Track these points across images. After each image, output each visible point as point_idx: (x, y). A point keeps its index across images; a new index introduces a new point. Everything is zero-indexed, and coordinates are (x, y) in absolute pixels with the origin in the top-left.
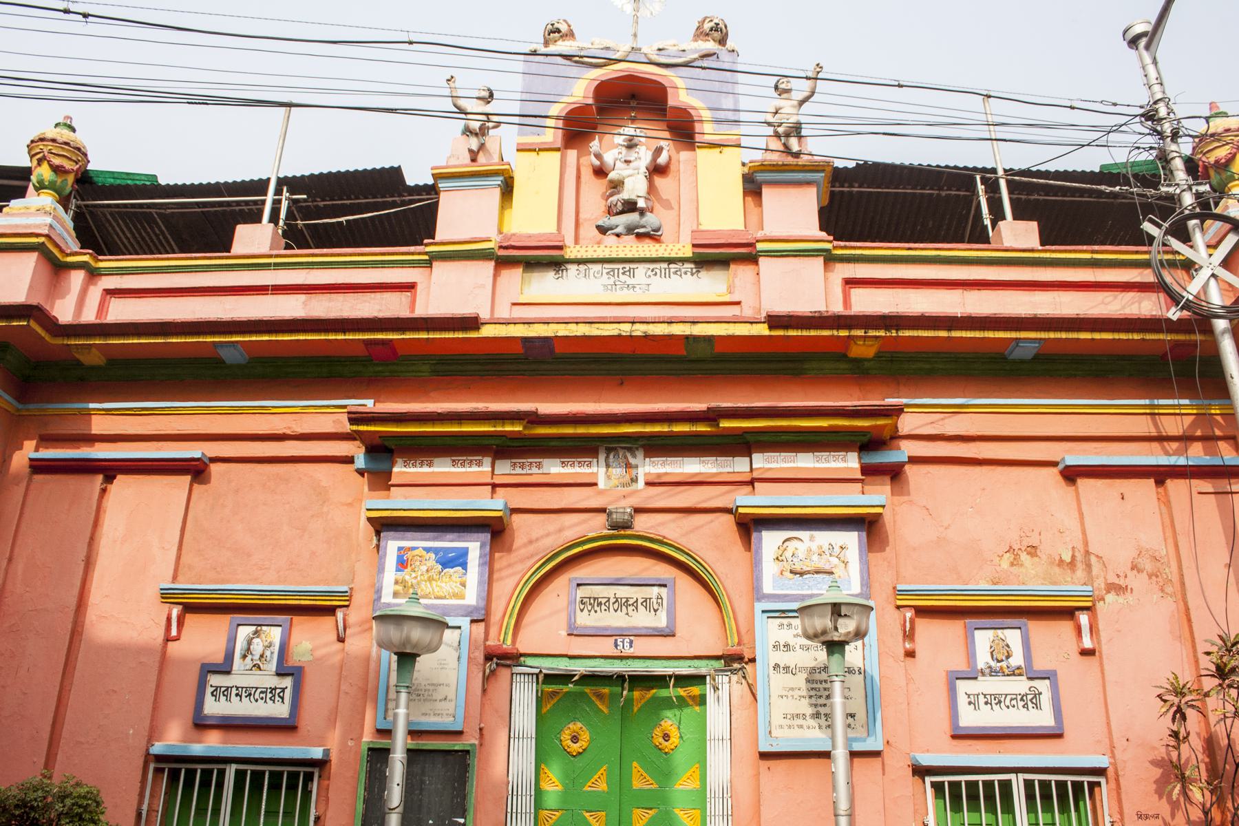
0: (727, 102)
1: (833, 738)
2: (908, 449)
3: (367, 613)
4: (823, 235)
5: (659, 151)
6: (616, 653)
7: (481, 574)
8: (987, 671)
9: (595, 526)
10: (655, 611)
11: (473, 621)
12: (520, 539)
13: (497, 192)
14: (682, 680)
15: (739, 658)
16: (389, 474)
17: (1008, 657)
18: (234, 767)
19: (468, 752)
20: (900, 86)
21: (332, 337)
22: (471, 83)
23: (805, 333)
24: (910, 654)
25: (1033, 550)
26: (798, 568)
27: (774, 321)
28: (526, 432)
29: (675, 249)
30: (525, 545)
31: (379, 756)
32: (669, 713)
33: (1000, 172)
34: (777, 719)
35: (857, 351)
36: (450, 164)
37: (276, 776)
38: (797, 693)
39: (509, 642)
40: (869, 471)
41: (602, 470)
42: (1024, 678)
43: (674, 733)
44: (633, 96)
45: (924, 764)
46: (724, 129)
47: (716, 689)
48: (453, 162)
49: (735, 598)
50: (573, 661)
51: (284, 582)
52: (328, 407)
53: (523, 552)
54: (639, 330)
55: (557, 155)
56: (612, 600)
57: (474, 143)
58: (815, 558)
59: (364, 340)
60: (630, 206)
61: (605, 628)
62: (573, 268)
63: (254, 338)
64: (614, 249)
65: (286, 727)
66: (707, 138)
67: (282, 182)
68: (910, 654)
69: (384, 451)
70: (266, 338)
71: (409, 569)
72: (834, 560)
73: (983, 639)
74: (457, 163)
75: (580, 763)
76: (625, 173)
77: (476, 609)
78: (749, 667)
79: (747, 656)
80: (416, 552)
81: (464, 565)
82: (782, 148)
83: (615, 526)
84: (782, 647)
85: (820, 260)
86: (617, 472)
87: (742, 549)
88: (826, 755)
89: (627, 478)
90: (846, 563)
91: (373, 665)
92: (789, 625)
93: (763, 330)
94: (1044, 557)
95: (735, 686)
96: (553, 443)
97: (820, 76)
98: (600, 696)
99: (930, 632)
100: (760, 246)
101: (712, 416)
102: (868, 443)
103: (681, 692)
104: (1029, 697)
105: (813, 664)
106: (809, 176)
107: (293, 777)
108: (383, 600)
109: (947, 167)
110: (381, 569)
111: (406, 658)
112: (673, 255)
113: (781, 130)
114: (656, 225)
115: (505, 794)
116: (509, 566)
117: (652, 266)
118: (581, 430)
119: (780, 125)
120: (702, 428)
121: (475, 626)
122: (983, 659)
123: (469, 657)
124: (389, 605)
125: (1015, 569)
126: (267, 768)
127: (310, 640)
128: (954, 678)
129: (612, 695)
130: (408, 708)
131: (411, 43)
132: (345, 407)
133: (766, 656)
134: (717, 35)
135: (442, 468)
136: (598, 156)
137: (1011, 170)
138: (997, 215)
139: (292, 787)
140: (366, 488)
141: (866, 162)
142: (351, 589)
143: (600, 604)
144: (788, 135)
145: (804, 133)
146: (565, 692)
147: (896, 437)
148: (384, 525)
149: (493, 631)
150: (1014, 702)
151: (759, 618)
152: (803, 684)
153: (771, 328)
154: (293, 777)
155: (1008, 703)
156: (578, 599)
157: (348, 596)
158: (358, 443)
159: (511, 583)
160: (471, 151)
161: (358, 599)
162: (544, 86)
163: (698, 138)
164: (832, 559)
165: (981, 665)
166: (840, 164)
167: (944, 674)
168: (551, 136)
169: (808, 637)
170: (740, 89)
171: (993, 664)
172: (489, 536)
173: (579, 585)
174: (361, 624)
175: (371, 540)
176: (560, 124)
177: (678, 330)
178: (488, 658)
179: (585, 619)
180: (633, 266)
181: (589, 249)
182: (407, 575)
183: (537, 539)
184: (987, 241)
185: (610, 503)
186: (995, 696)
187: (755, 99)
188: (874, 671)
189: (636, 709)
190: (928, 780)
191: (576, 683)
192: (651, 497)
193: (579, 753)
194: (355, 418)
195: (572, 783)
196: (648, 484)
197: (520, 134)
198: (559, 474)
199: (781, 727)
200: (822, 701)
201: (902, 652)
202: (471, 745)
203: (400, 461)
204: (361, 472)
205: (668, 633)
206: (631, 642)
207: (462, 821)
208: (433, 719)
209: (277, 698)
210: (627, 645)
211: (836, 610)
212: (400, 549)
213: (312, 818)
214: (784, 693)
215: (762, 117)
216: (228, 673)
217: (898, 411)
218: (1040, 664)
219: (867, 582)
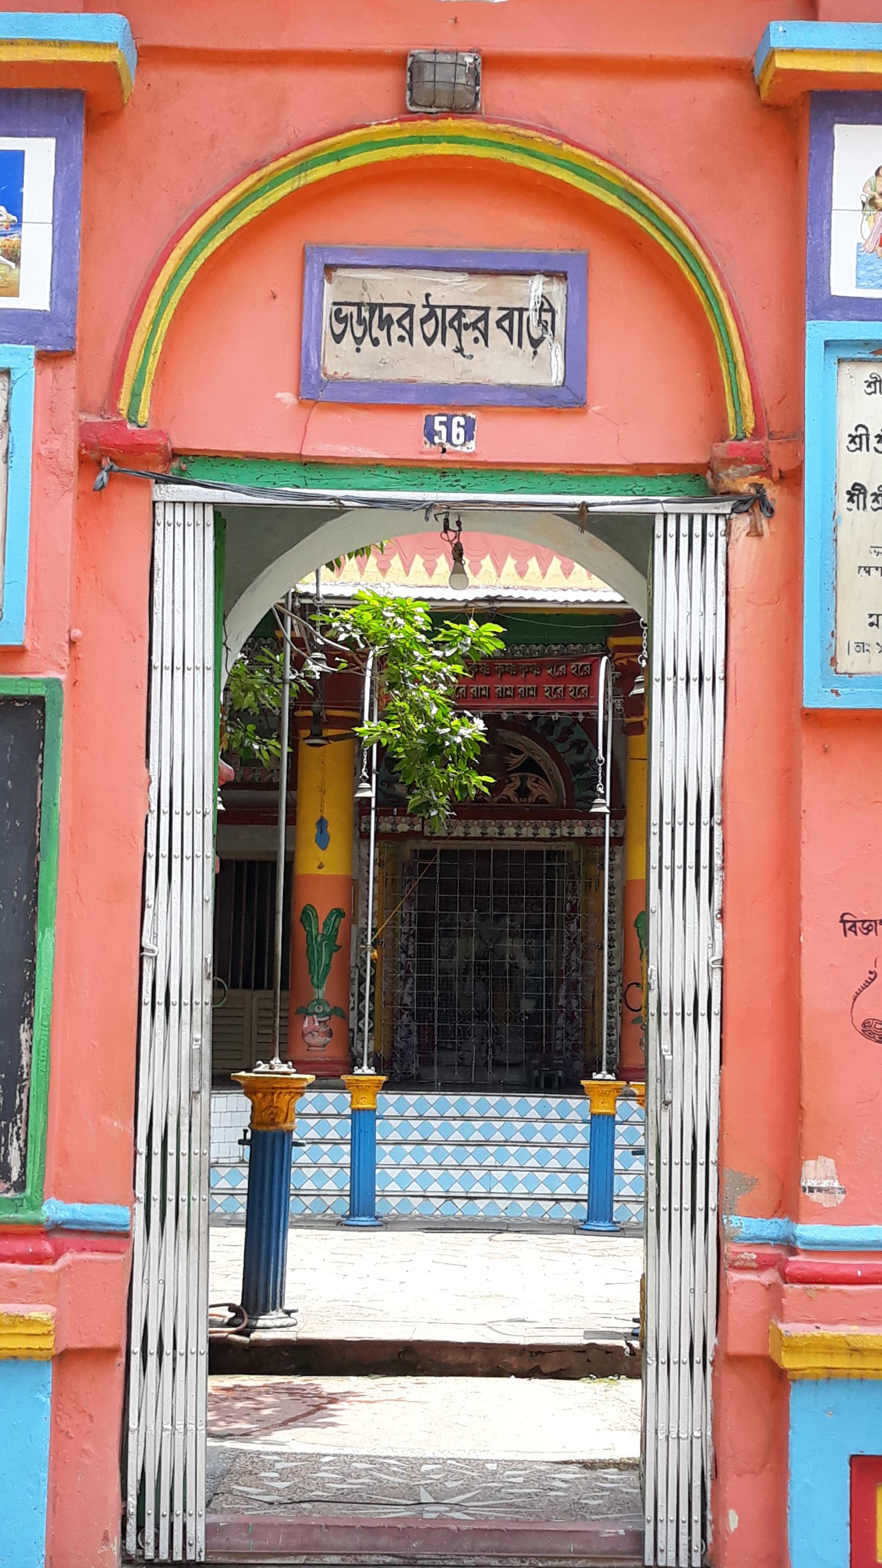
6: (429, 452)
10: (535, 343)
19: (39, 702)
34: (852, 626)
56: (420, 313)
123: (37, 455)
143: (386, 323)
156: (328, 308)
179: (342, 360)
199: (862, 647)
202: (48, 683)
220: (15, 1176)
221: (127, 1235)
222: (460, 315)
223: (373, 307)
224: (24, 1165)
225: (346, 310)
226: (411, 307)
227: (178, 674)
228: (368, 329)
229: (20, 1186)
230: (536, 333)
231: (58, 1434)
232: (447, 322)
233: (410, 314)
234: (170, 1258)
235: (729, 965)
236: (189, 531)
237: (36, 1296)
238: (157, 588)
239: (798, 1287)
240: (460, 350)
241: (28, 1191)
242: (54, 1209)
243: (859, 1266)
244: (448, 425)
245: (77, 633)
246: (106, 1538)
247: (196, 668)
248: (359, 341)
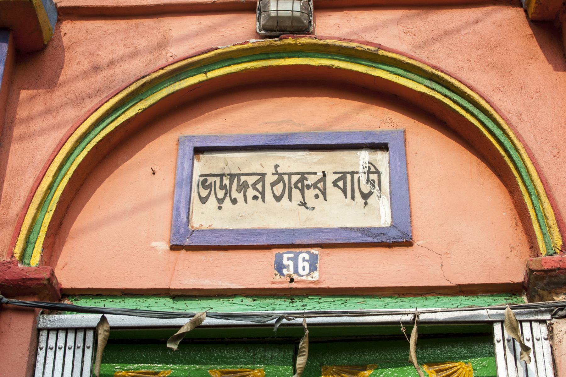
6: (281, 283)
10: (366, 196)
12: (74, 64)
30: (85, 74)
39: (35, 259)
53: (80, 86)
56: (270, 179)
116: (48, 111)
143: (243, 187)
156: (196, 178)
159: (49, 142)
173: (198, 151)
179: (208, 217)
183: (111, 64)
205: (397, 240)
223: (232, 177)
225: (210, 180)
226: (263, 175)
228: (228, 192)
230: (366, 189)
232: (298, 185)
236: (69, 353)
240: (303, 204)
244: (295, 260)
248: (220, 201)
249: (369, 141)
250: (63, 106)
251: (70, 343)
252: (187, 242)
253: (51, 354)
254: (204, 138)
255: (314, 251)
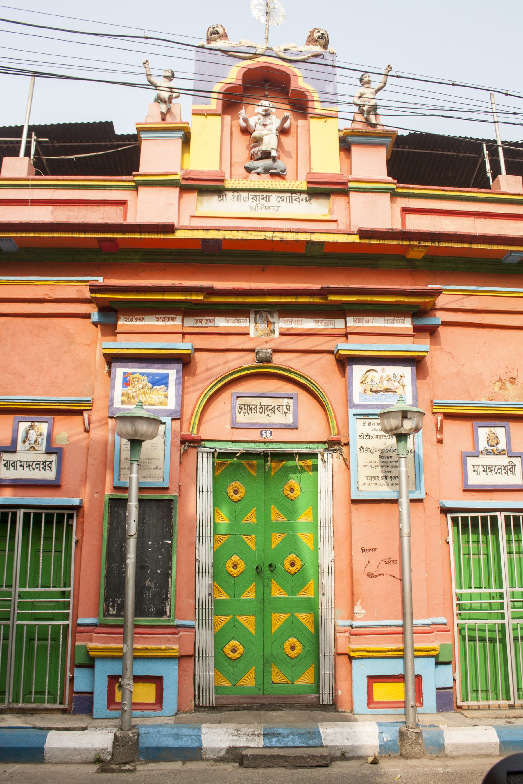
0: (329, 88)
1: (399, 492)
2: (441, 316)
3: (104, 413)
4: (390, 179)
5: (285, 119)
6: (262, 439)
7: (177, 390)
8: (485, 452)
9: (248, 361)
10: (286, 413)
11: (173, 419)
12: (200, 368)
13: (180, 142)
14: (304, 456)
15: (338, 443)
16: (115, 326)
17: (497, 444)
18: (22, 511)
19: (172, 500)
20: (453, 85)
21: (76, 235)
22: (159, 66)
23: (382, 242)
24: (440, 441)
25: (513, 381)
26: (374, 388)
27: (363, 234)
28: (205, 300)
29: (296, 185)
30: (204, 372)
31: (118, 504)
32: (294, 476)
33: (499, 143)
34: (362, 480)
35: (412, 255)
36: (148, 121)
37: (49, 517)
38: (374, 464)
39: (195, 432)
40: (418, 330)
41: (252, 325)
42: (506, 456)
43: (297, 488)
44: (266, 81)
45: (448, 507)
46: (328, 106)
47: (324, 461)
48: (149, 120)
49: (335, 406)
50: (234, 444)
51: (48, 394)
52: (73, 281)
53: (203, 376)
54: (278, 236)
55: (219, 118)
56: (259, 407)
57: (164, 108)
58: (385, 382)
59: (98, 238)
60: (266, 155)
61: (255, 424)
62: (230, 194)
63: (24, 235)
64: (257, 183)
65: (53, 486)
66: (317, 111)
67: (32, 128)
68: (440, 441)
69: (111, 312)
70: (32, 235)
71: (131, 386)
72: (397, 384)
73: (483, 433)
74: (152, 121)
75: (239, 506)
76: (264, 132)
77: (175, 412)
78: (344, 449)
79: (343, 441)
80: (135, 376)
81: (166, 384)
82: (364, 121)
83: (261, 361)
84: (367, 437)
85: (388, 196)
86: (262, 326)
87: (339, 376)
88: (395, 501)
89: (268, 331)
90: (403, 386)
91: (109, 447)
92: (369, 423)
93: (355, 239)
94: (519, 385)
95: (336, 460)
96: (221, 308)
97: (390, 74)
98: (251, 466)
99: (452, 428)
100: (351, 185)
101: (323, 293)
102: (418, 312)
103: (301, 463)
104: (509, 467)
105: (383, 447)
106: (382, 140)
107: (60, 517)
108: (115, 406)
109: (466, 138)
110: (113, 387)
111: (136, 443)
112: (295, 188)
113: (365, 108)
114: (283, 169)
115: (194, 526)
116: (194, 385)
117: (281, 195)
118: (240, 300)
119: (364, 105)
120: (316, 300)
121: (174, 422)
122: (483, 445)
123: (171, 442)
124: (118, 409)
125: (502, 392)
126: (44, 511)
127: (67, 431)
128: (465, 456)
129: (258, 465)
130: (138, 473)
131: (146, 38)
132: (87, 281)
133: (356, 442)
134: (322, 42)
135: (150, 322)
136: (245, 120)
137: (506, 142)
138: (496, 172)
139: (60, 523)
140: (99, 335)
141: (421, 133)
142: (93, 399)
143: (251, 409)
144: (368, 113)
145: (378, 111)
146: (231, 463)
147: (434, 309)
148: (112, 359)
149: (185, 425)
150: (500, 471)
151: (351, 418)
152: (377, 459)
153: (361, 238)
154: (60, 517)
155: (496, 471)
156: (237, 406)
157: (90, 403)
158: (94, 305)
159: (195, 395)
160: (162, 113)
161: (97, 405)
162: (211, 69)
163: (310, 110)
164: (395, 383)
165: (481, 448)
166: (400, 133)
167: (459, 454)
168: (215, 105)
169: (386, 431)
170: (338, 79)
171: (488, 448)
172: (181, 366)
173: (238, 397)
174: (100, 420)
175: (104, 368)
176: (221, 96)
177: (302, 237)
178: (183, 442)
179: (242, 418)
180: (268, 194)
181: (241, 182)
182: (129, 390)
183: (211, 368)
184: (489, 187)
185: (257, 346)
186: (489, 467)
187: (347, 87)
188: (420, 451)
189: (273, 473)
190: (449, 516)
191: (238, 458)
192: (283, 343)
193: (239, 500)
194: (95, 289)
195: (235, 518)
196: (281, 334)
197: (194, 103)
198: (225, 327)
199: (364, 484)
200: (389, 469)
201: (435, 440)
202: (174, 496)
203: (122, 317)
204: (95, 324)
205: (294, 428)
206: (271, 433)
207: (170, 542)
208: (149, 480)
209: (47, 468)
210: (268, 434)
211: (405, 415)
212: (124, 373)
213: (74, 542)
214: (367, 464)
215: (351, 100)
216: (14, 452)
217: (437, 293)
218: (516, 448)
219: (415, 398)
220: (168, 614)
221: (194, 628)
222: (268, 407)
223: (248, 406)
224: (170, 612)
225: (241, 406)
226: (257, 405)
227: (204, 493)
228: (247, 411)
229: (170, 616)
230: (286, 411)
231: (180, 676)
232: (266, 409)
233: (256, 407)
234: (204, 633)
235: (335, 560)
236: (206, 459)
237: (174, 643)
238: (198, 472)
239: (354, 636)
240: (268, 415)
241: (171, 618)
242: (177, 622)
243: (368, 631)
244: (266, 433)
245: (180, 484)
246: (191, 701)
247: (208, 491)
248: (245, 413)
249: (287, 396)
250: (198, 383)
251: (206, 456)
252: (236, 427)
253: (201, 459)
254: (239, 393)
255: (271, 430)
